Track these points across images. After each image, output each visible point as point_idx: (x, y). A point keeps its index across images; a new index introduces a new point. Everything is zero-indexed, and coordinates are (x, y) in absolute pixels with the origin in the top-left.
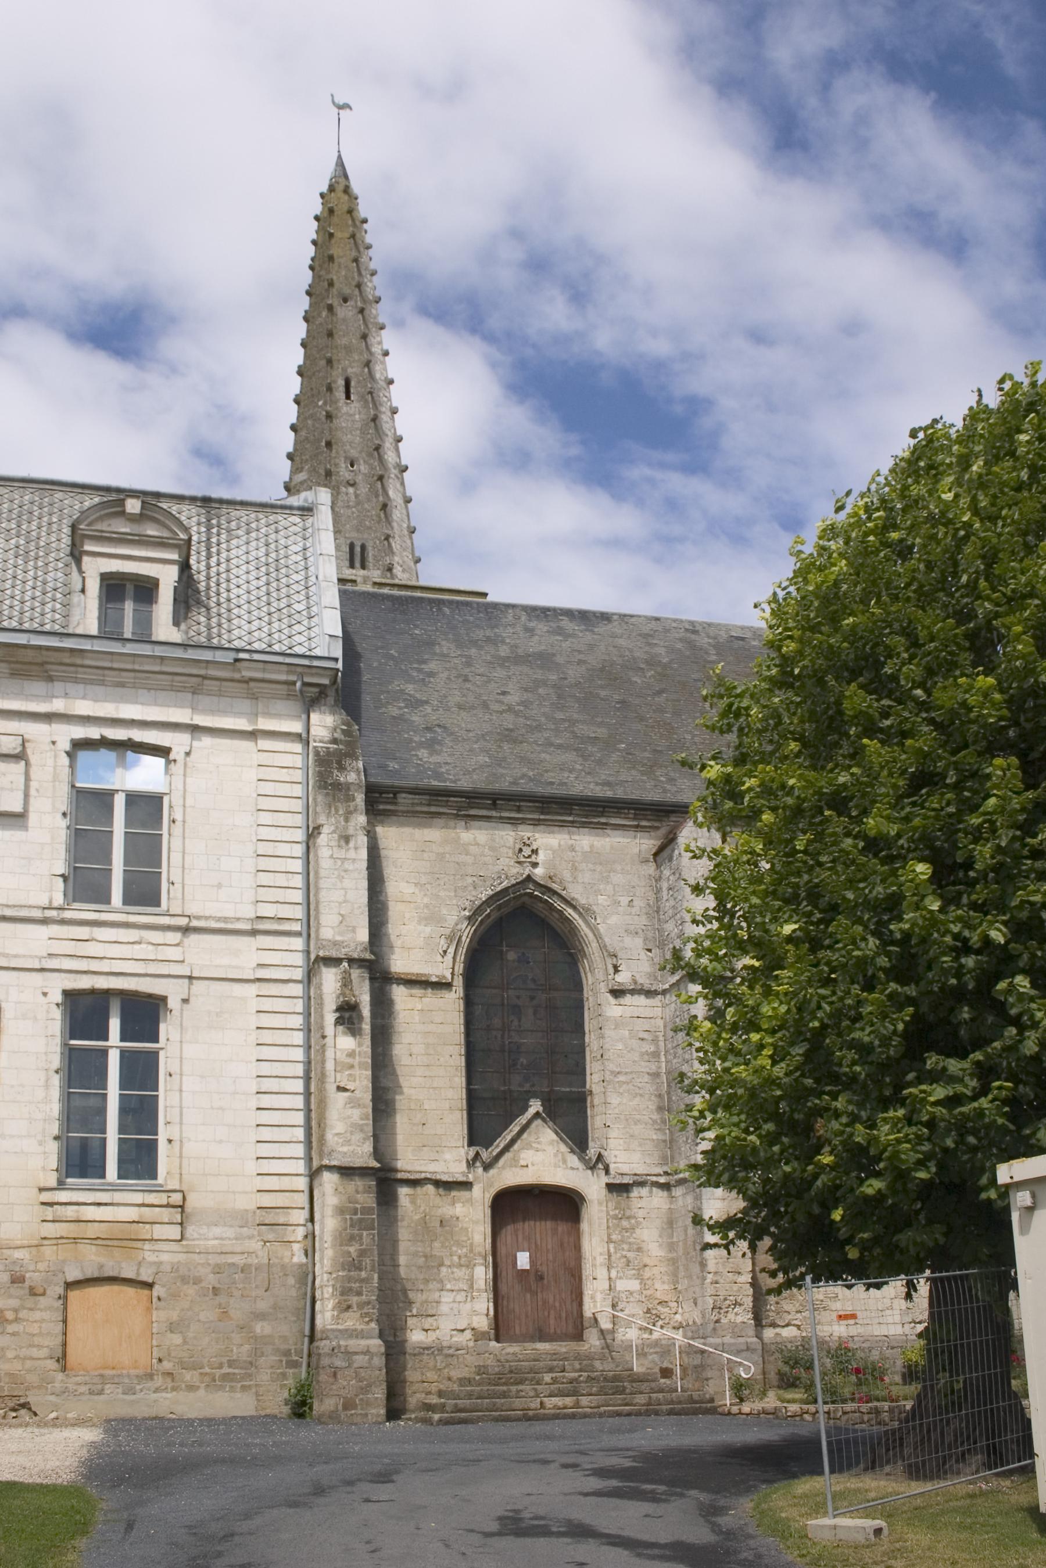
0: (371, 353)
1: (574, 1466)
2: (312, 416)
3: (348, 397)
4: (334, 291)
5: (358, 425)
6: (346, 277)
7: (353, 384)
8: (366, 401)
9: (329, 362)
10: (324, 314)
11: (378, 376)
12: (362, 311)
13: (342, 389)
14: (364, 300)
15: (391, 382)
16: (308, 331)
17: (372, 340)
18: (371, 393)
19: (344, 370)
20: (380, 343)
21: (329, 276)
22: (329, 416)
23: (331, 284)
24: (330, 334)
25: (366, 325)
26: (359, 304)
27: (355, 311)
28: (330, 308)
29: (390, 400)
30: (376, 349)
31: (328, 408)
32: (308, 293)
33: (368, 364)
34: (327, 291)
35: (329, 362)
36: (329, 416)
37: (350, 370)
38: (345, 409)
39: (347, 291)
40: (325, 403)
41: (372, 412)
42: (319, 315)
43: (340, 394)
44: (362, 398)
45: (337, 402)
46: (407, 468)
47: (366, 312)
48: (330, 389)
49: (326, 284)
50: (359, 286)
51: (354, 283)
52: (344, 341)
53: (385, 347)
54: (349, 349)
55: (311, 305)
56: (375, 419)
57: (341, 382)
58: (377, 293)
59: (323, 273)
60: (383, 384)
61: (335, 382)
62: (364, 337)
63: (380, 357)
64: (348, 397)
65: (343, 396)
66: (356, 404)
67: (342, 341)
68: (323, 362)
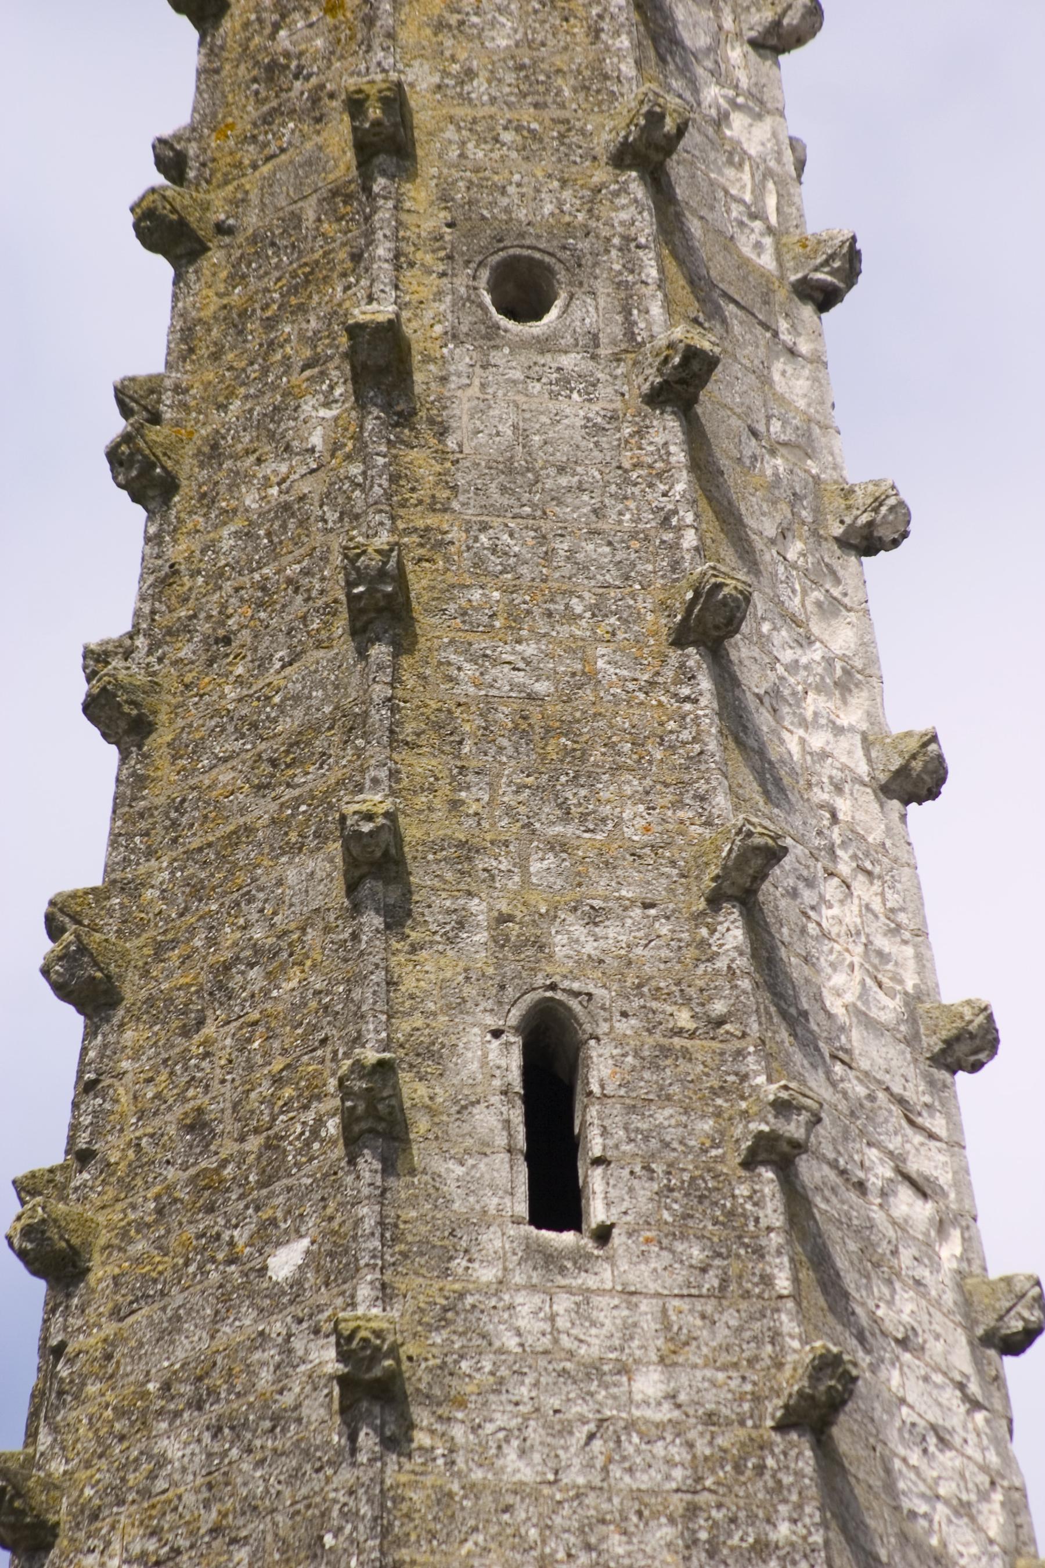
0: (772, 780)
1: (882, 1332)
2: (196, 1387)
3: (555, 1198)
4: (420, 204)
5: (660, 1468)
6: (530, 76)
7: (601, 1068)
8: (736, 1232)
9: (376, 866)
10: (321, 416)
11: (839, 988)
12: (682, 385)
13: (499, 1121)
14: (705, 295)
15: (970, 1045)
16: (161, 581)
17: (765, 653)
18: (775, 1154)
19: (519, 938)
20: (849, 678)
21: (367, 72)
22: (374, 1390)
23: (386, 141)
24: (381, 611)
25: (729, 520)
26: (661, 325)
27: (622, 386)
28: (381, 365)
29: (956, 1219)
30: (824, 742)
31: (367, 1311)
32: (162, 229)
33: (744, 881)
34: (352, 199)
35: (376, 866)
36: (374, 1390)
37: (571, 941)
38: (525, 1317)
39: (535, 201)
40: (334, 1262)
41: (799, 1346)
42: (273, 429)
43: (481, 1167)
44: (694, 1199)
45: (444, 1250)
46: (849, 262)
47: (722, 397)
48: (378, 1123)
49: (337, 137)
50: (650, 153)
51: (607, 131)
52: (517, 669)
53: (905, 716)
54: (558, 744)
55: (186, 339)
56: (820, 1409)
57: (490, 1062)
58: (825, 211)
59: (303, 36)
60: (884, 1059)
61: (432, 1054)
62: (710, 625)
63: (861, 809)
64: (555, 1198)
65: (502, 1183)
66: (629, 1265)
67: (481, 663)
68: (314, 876)
